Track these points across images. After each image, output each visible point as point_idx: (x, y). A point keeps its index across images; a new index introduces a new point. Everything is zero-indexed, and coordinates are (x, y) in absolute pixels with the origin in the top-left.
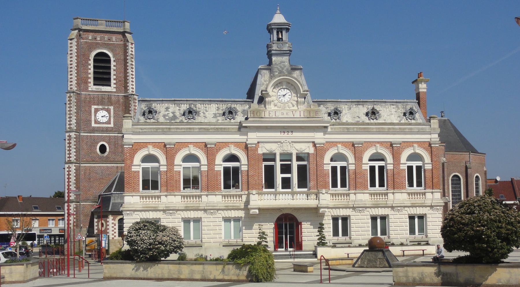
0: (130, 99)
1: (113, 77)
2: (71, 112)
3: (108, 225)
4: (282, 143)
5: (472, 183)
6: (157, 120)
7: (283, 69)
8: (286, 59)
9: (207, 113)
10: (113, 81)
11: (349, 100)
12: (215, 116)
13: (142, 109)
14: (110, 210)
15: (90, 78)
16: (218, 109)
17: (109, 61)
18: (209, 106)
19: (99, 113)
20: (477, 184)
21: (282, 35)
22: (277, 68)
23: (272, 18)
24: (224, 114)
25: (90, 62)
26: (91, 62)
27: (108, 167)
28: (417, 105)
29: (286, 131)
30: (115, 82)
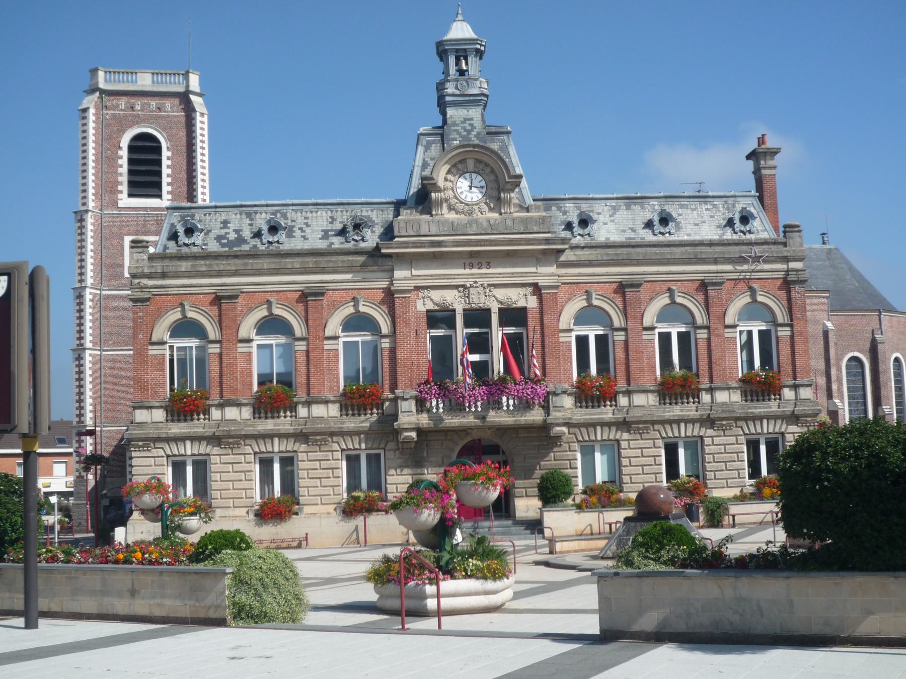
1: (165, 180)
7: (469, 132)
8: (475, 113)
9: (308, 230)
10: (166, 188)
11: (611, 196)
12: (326, 235)
15: (121, 183)
16: (333, 220)
17: (158, 150)
18: (314, 214)
22: (457, 131)
23: (447, 29)
25: (120, 153)
26: (124, 153)
28: (756, 202)
29: (475, 261)
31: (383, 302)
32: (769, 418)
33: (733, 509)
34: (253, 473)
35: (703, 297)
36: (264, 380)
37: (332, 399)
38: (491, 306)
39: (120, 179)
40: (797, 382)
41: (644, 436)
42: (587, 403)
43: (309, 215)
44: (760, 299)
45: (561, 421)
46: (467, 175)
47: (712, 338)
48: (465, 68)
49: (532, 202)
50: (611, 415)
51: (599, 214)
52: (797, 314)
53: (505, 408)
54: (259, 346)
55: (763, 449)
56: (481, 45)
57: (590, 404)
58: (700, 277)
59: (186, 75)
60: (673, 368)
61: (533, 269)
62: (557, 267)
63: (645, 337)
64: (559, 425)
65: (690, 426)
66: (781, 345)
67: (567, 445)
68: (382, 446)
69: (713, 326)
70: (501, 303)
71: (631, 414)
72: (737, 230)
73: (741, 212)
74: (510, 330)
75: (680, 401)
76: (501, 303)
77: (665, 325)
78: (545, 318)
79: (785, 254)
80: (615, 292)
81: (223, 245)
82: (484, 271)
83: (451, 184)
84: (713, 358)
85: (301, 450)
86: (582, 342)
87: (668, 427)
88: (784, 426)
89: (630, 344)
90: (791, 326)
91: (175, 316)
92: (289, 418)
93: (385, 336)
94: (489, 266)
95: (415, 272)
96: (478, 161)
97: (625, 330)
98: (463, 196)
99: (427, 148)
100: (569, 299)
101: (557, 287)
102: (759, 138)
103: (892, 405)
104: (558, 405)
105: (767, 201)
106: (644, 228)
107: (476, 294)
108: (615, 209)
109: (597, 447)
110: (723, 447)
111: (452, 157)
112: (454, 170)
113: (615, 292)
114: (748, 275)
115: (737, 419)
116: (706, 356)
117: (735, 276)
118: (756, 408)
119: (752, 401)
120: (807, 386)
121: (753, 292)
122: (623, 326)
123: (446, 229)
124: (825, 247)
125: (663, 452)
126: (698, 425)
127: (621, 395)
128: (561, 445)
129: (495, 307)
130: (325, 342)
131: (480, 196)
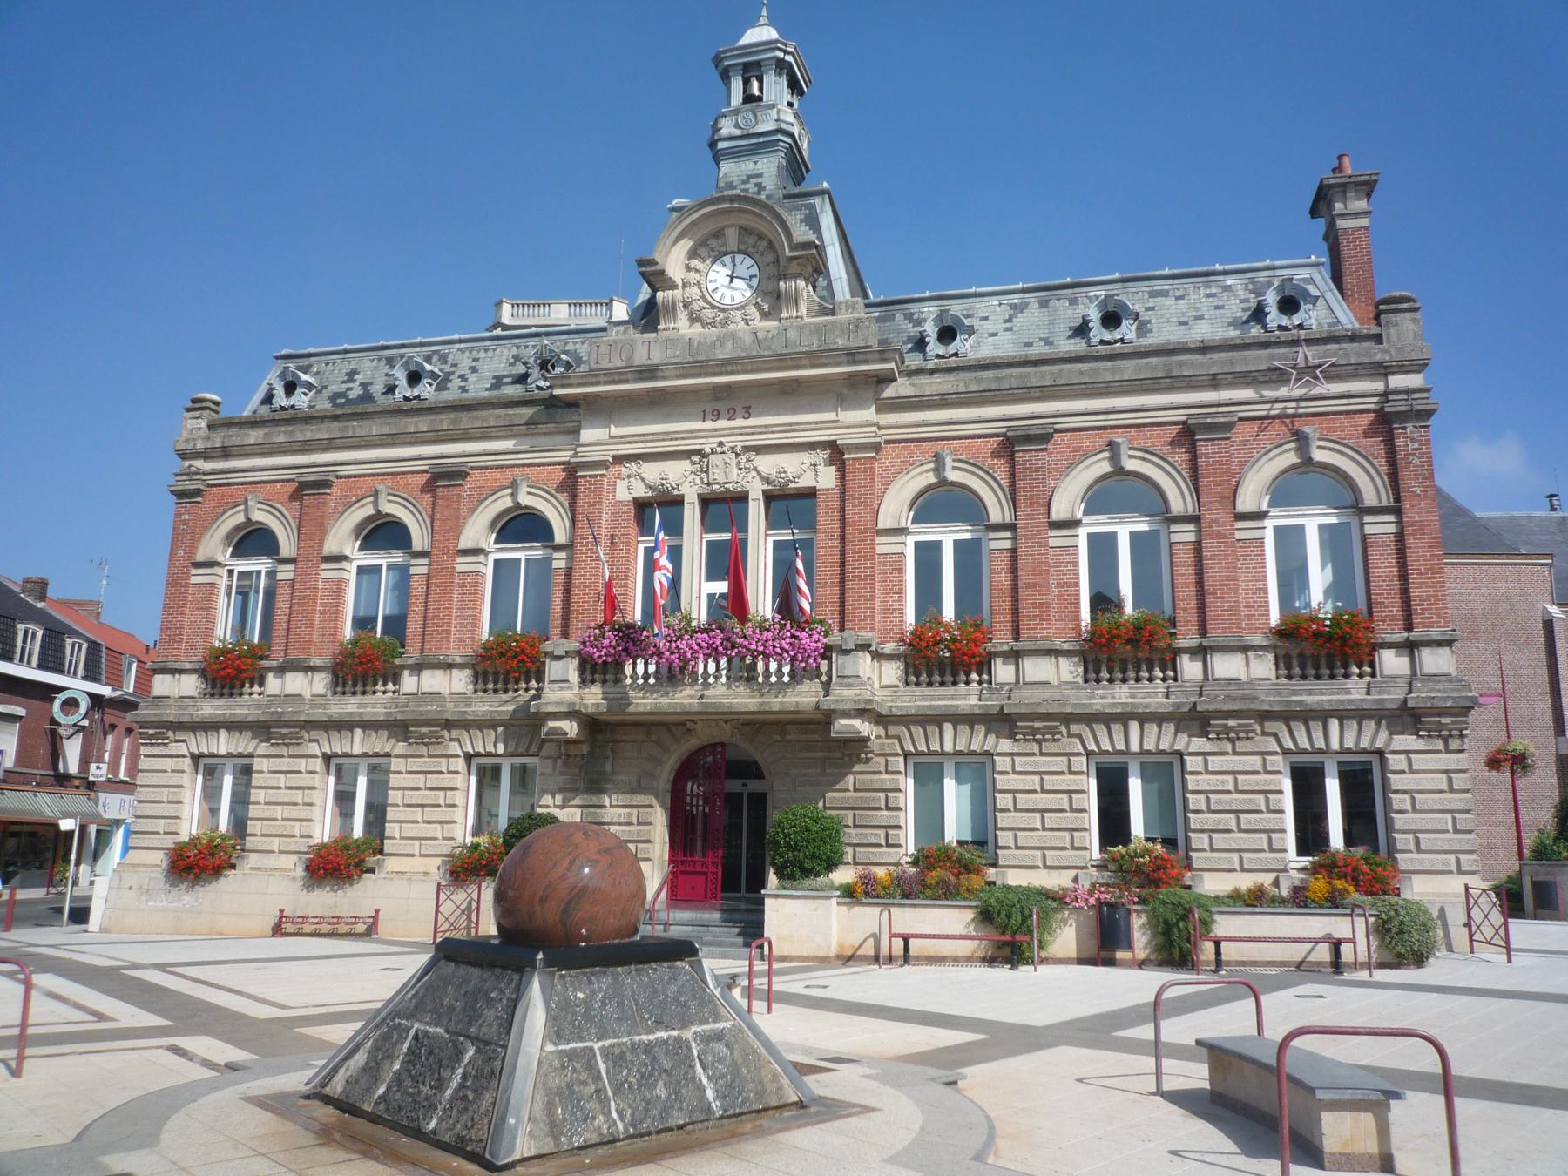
4: (707, 456)
21: (761, 89)
31: (562, 487)
32: (1343, 715)
33: (1225, 925)
34: (902, 814)
35: (1186, 457)
36: (363, 623)
37: (458, 660)
38: (748, 487)
40: (1414, 636)
41: (1046, 747)
42: (930, 675)
43: (482, 355)
44: (1319, 456)
45: (848, 706)
46: (727, 259)
47: (1206, 540)
48: (757, 93)
50: (974, 701)
52: (1411, 484)
53: (760, 680)
54: (361, 570)
55: (1333, 787)
56: (786, 52)
57: (937, 678)
58: (1179, 416)
59: (609, 305)
60: (1119, 607)
61: (830, 416)
62: (879, 411)
64: (846, 714)
65: (1152, 729)
66: (1373, 555)
67: (882, 760)
69: (1207, 517)
70: (768, 481)
71: (1016, 698)
72: (1272, 325)
73: (1280, 289)
74: (785, 535)
75: (1132, 675)
76: (768, 481)
77: (1102, 518)
78: (849, 506)
79: (1378, 358)
80: (995, 454)
82: (739, 422)
83: (697, 276)
84: (1208, 582)
85: (396, 752)
86: (928, 555)
87: (1101, 730)
88: (1383, 735)
89: (1021, 555)
90: (1397, 512)
91: (235, 518)
92: (390, 694)
93: (558, 548)
94: (748, 413)
95: (615, 431)
96: (745, 231)
97: (1011, 527)
98: (717, 296)
100: (900, 471)
101: (876, 447)
104: (847, 673)
105: (1349, 280)
106: (1070, 337)
107: (721, 465)
109: (949, 768)
110: (1230, 778)
111: (693, 223)
112: (703, 251)
113: (995, 454)
114: (1291, 408)
115: (1264, 716)
116: (1192, 579)
117: (1260, 410)
118: (1310, 693)
119: (1304, 677)
120: (1440, 644)
121: (1301, 440)
122: (1008, 520)
123: (678, 355)
124: (1554, 514)
126: (1172, 727)
127: (999, 661)
128: (868, 760)
129: (756, 490)
130: (460, 559)
131: (748, 293)
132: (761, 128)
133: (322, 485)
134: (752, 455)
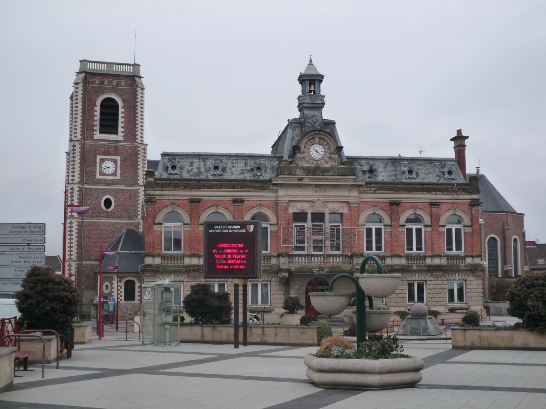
0: (139, 149)
1: (120, 125)
2: (75, 163)
3: (114, 288)
5: (510, 245)
6: (181, 176)
7: (315, 122)
9: (234, 169)
10: (120, 130)
12: (243, 172)
13: (164, 163)
14: (527, 247)
16: (246, 165)
17: (117, 107)
19: (113, 164)
20: (515, 248)
21: (315, 88)
22: (310, 123)
24: (252, 169)
25: (96, 108)
26: (98, 109)
27: (113, 223)
30: (123, 130)
39: (95, 123)
43: (234, 161)
49: (346, 160)
51: (378, 167)
58: (428, 201)
63: (400, 230)
68: (270, 280)
69: (433, 226)
81: (191, 175)
96: (321, 139)
99: (294, 130)
100: (363, 210)
102: (458, 131)
103: (512, 265)
108: (386, 165)
125: (407, 287)
132: (317, 102)
133: (242, 201)
134: (326, 203)
